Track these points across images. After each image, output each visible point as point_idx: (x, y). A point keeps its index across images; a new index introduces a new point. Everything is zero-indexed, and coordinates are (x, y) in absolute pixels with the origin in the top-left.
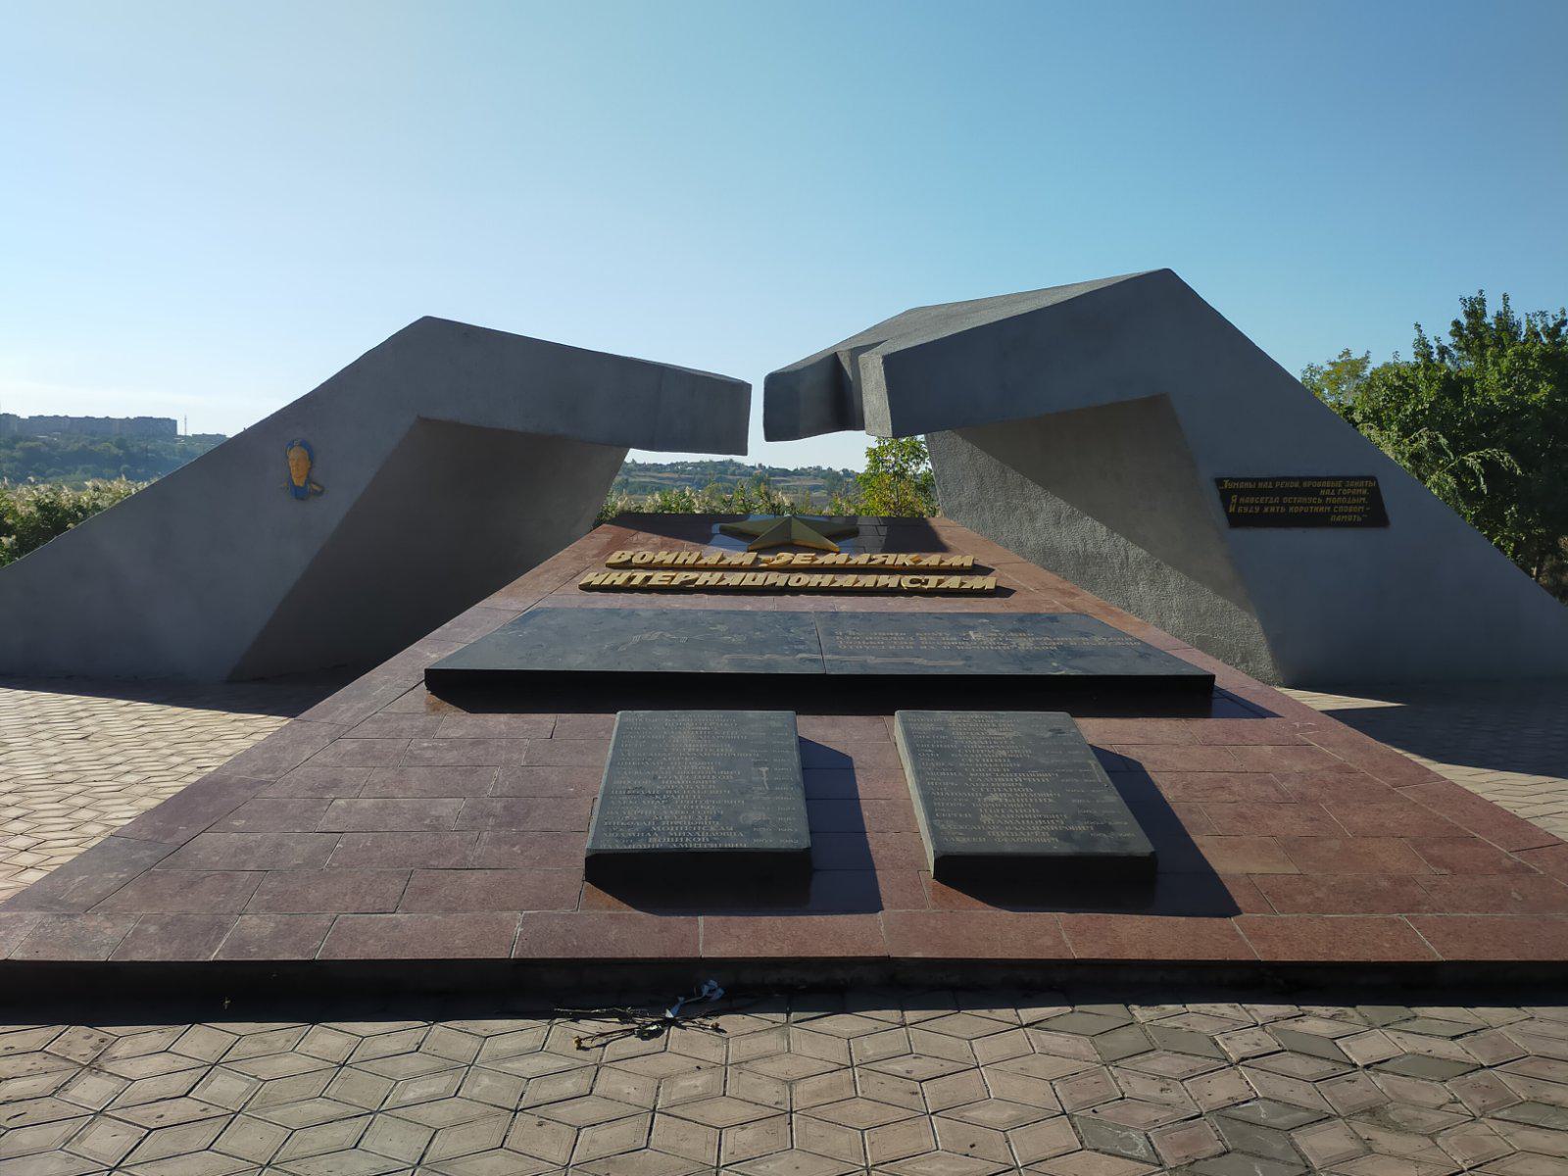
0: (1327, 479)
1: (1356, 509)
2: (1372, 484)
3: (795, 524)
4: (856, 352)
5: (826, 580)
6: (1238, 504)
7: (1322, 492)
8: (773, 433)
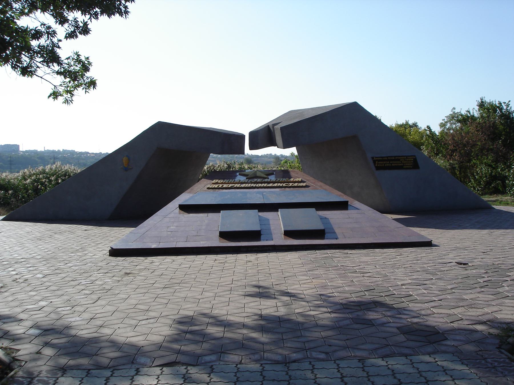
0: (401, 156)
1: (410, 164)
2: (414, 157)
3: (257, 172)
4: (274, 125)
5: (265, 185)
6: (378, 164)
7: (401, 160)
8: (251, 148)
